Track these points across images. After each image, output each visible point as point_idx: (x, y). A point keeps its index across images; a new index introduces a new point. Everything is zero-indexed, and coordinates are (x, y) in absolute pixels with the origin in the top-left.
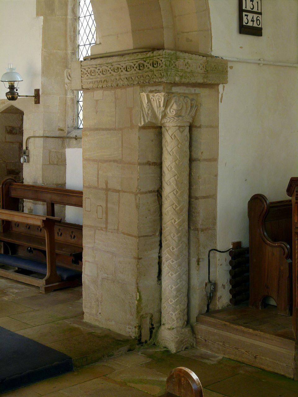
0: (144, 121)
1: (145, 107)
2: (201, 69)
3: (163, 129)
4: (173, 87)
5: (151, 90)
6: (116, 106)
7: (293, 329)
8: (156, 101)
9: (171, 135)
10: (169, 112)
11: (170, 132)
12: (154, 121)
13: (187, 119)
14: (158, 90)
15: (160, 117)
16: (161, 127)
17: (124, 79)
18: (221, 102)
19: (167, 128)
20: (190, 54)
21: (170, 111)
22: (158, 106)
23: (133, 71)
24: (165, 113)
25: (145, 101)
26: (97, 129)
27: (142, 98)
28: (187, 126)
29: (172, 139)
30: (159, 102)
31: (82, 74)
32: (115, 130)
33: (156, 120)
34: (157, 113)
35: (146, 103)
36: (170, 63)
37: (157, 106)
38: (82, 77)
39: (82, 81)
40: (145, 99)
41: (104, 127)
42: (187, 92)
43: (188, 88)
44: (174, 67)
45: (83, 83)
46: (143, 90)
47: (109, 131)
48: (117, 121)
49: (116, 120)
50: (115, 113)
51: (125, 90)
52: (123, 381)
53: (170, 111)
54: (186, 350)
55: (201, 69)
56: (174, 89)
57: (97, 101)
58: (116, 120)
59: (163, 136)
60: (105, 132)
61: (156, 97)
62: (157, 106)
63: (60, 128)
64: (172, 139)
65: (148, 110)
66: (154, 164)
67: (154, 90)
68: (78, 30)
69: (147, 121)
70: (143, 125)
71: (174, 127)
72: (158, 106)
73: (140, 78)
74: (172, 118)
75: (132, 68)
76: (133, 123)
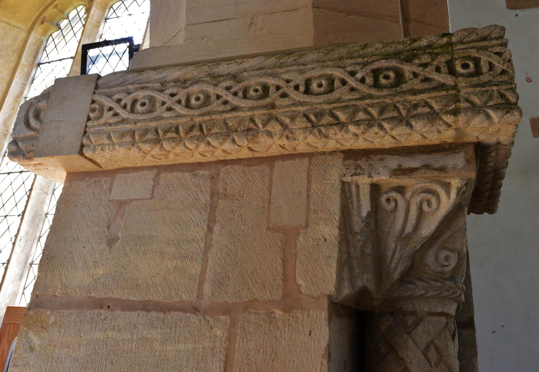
5: (400, 165)
7: (393, 245)
9: (423, 346)
11: (423, 335)
19: (410, 320)
21: (437, 258)
25: (359, 207)
26: (100, 304)
31: (93, 110)
32: (195, 310)
33: (59, 271)
34: (389, 253)
38: (89, 119)
39: (85, 132)
41: (136, 297)
45: (89, 138)
46: (357, 167)
47: (161, 315)
48: (209, 274)
50: (202, 245)
51: (268, 170)
52: (50, 168)
53: (437, 258)
57: (121, 204)
58: (203, 272)
63: (17, 279)
67: (417, 166)
68: (100, 33)
76: (299, 286)
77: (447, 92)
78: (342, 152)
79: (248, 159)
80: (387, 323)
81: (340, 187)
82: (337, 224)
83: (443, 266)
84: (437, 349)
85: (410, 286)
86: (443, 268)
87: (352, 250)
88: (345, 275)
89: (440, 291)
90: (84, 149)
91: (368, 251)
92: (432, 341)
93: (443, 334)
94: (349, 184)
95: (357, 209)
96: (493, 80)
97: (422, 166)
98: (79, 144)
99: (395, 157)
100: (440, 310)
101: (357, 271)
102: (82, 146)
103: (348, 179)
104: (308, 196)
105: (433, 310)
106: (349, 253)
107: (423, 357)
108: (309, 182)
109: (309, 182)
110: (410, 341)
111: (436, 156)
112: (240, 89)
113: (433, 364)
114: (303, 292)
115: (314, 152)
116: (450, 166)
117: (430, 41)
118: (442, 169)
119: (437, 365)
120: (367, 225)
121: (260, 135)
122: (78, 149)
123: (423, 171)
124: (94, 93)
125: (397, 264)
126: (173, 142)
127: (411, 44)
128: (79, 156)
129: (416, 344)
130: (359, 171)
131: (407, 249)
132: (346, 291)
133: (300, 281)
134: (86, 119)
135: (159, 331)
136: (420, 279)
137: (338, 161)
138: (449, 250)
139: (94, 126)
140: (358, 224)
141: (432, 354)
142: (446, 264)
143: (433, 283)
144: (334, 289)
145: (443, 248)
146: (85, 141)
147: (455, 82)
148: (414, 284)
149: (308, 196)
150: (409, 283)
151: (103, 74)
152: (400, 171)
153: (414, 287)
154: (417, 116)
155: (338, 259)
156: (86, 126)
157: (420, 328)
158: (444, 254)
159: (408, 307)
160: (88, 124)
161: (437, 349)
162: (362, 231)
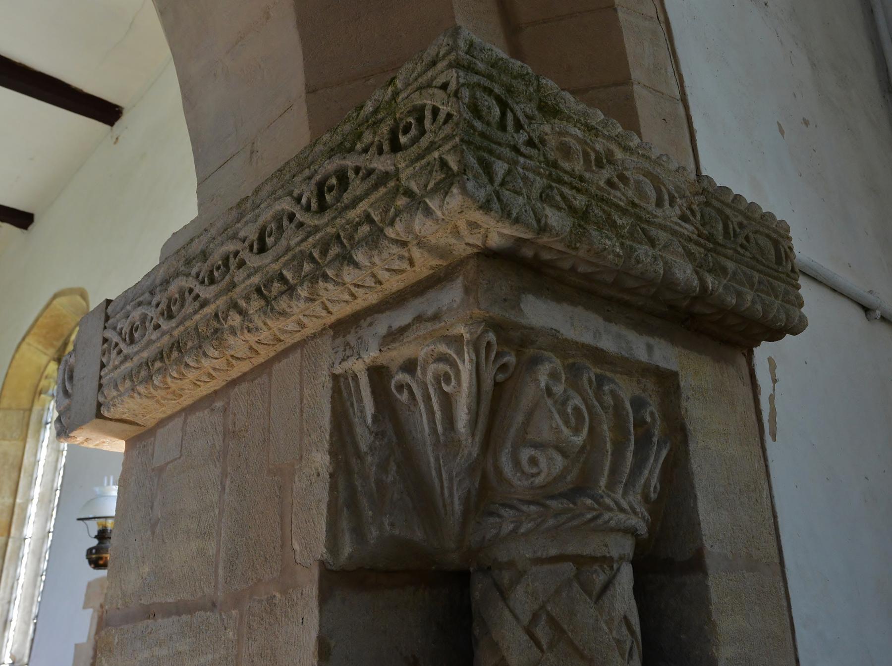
0: (358, 532)
1: (363, 447)
2: (684, 218)
3: (479, 586)
4: (531, 298)
6: (224, 474)
8: (427, 398)
9: (526, 620)
10: (508, 469)
11: (523, 599)
12: (418, 535)
13: (622, 510)
14: (430, 312)
15: (458, 507)
16: (460, 579)
17: (247, 299)
18: (774, 439)
19: (506, 577)
20: (544, 556)
21: (517, 464)
22: (440, 428)
23: (292, 238)
24: (484, 477)
25: (362, 411)
26: (149, 613)
27: (345, 394)
28: (622, 558)
29: (538, 644)
30: (447, 402)
34: (436, 482)
35: (369, 420)
36: (503, 115)
37: (434, 430)
38: (103, 366)
39: (100, 386)
40: (360, 400)
42: (607, 344)
43: (614, 328)
44: (530, 143)
49: (218, 551)
53: (517, 464)
54: (459, 95)
55: (684, 218)
56: (540, 313)
59: (477, 631)
60: (166, 625)
61: (424, 370)
62: (434, 430)
64: (538, 644)
65: (383, 467)
66: (24, 410)
69: (373, 534)
70: (351, 557)
71: (546, 567)
72: (440, 428)
73: (324, 252)
74: (533, 508)
75: (285, 222)
77: (386, 187)
78: (331, 326)
79: (252, 371)
80: (480, 586)
81: (331, 385)
82: (327, 446)
83: (533, 475)
84: (553, 622)
85: (492, 520)
86: (532, 479)
87: (358, 482)
88: (345, 524)
89: (539, 520)
90: (102, 408)
91: (390, 478)
92: (543, 607)
93: (564, 595)
94: (345, 376)
95: (359, 414)
96: (436, 140)
97: (414, 319)
98: (95, 403)
99: (384, 315)
100: (553, 552)
101: (370, 513)
102: (99, 405)
103: (338, 370)
104: (302, 411)
105: (539, 554)
106: (351, 488)
107: (526, 637)
108: (302, 388)
109: (302, 388)
110: (507, 613)
111: (431, 295)
112: (314, 246)
113: (545, 647)
114: (298, 561)
115: (304, 337)
116: (445, 308)
117: (375, 100)
118: (436, 317)
119: (551, 646)
120: (379, 435)
121: (225, 336)
122: (94, 411)
123: (415, 327)
124: (105, 328)
125: (451, 489)
126: (159, 374)
127: (357, 116)
128: (98, 420)
129: (516, 617)
130: (348, 352)
131: (458, 461)
132: (347, 549)
133: (296, 547)
134: (99, 367)
135: (188, 640)
136: (504, 505)
137: (326, 344)
138: (532, 446)
139: (106, 375)
140: (364, 438)
141: (542, 632)
142: (534, 470)
143: (525, 508)
144: (324, 550)
145: (522, 441)
146: (101, 399)
147: (395, 165)
148: (500, 516)
149: (302, 411)
150: (491, 514)
151: (112, 297)
152: (394, 336)
153: (498, 520)
154: (355, 245)
155: (330, 501)
156: (101, 377)
157: (520, 590)
158: (526, 454)
159: (502, 555)
160: (102, 374)
161: (553, 622)
162: (371, 448)
